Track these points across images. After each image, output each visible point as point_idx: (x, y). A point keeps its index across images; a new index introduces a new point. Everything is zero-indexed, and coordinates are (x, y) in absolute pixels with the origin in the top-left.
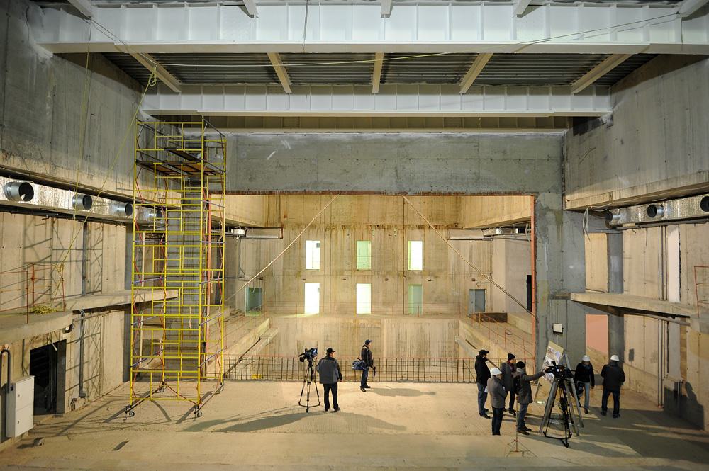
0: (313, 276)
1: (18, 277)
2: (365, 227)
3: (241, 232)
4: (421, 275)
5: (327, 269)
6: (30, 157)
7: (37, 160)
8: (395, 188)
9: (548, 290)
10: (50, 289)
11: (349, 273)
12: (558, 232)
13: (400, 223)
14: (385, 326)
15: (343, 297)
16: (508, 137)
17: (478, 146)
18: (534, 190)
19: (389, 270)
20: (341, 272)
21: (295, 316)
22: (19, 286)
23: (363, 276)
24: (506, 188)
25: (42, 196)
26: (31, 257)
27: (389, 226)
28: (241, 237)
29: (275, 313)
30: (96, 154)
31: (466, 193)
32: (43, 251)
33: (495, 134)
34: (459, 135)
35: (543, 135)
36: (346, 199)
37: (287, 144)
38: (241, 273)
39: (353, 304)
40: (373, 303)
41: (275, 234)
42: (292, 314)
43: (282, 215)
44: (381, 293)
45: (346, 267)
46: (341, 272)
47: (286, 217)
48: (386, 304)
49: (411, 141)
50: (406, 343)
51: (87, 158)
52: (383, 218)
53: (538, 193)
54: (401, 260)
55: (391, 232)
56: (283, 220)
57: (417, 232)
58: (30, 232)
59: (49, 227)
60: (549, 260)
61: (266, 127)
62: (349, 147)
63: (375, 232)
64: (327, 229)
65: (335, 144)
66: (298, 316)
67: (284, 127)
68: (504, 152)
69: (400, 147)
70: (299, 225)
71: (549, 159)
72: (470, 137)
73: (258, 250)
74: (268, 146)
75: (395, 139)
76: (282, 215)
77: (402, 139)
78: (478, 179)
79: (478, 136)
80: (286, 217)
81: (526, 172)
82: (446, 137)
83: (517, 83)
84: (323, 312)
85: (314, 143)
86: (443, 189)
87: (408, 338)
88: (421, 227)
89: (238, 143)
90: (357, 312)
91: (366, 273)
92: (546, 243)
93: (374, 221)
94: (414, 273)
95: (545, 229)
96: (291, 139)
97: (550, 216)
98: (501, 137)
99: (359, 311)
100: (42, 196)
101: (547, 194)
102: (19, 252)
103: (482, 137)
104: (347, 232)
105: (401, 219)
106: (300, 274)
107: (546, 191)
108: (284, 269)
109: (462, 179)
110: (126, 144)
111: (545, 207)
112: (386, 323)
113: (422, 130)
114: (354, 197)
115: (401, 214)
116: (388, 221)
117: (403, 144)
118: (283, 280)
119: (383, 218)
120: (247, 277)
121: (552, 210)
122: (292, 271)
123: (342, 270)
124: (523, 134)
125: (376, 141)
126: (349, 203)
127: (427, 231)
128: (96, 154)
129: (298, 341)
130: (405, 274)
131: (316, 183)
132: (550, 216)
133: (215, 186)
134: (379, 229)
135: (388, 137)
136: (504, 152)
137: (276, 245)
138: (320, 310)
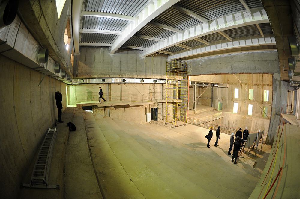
0: (236, 100)
1: (148, 95)
2: (251, 85)
3: (217, 85)
4: (268, 103)
5: (240, 98)
6: (142, 75)
7: (143, 75)
8: (231, 72)
9: (275, 111)
10: (155, 98)
11: (246, 100)
12: (280, 89)
13: (262, 84)
14: (253, 120)
15: (244, 108)
16: (262, 52)
17: (254, 56)
18: (272, 72)
19: (258, 100)
20: (244, 100)
21: (228, 113)
22: (149, 97)
23: (251, 102)
24: (264, 71)
25: (146, 81)
26: (150, 91)
27: (259, 84)
28: (217, 87)
29: (225, 111)
30: (156, 72)
31: (252, 73)
32: (153, 90)
33: (258, 52)
34: (248, 53)
35: (272, 51)
36: (246, 75)
37: (203, 61)
38: (217, 98)
39: (247, 111)
40: (253, 112)
41: (225, 86)
42: (229, 112)
43: (228, 80)
44: (255, 109)
45: (246, 98)
46: (244, 100)
47: (229, 80)
48: (256, 112)
49: (234, 56)
50: (258, 127)
51: (154, 73)
52: (257, 82)
53: (273, 73)
54: (262, 97)
55: (259, 87)
56: (228, 81)
57: (267, 87)
58: (150, 87)
59: (154, 86)
60: (277, 100)
61: (198, 57)
62: (218, 60)
63: (255, 86)
64: (240, 86)
65: (215, 59)
66: (232, 113)
67: (196, 57)
68: (262, 58)
69: (232, 58)
70: (232, 83)
71: (275, 60)
72: (251, 53)
73: (222, 91)
74: (199, 62)
75: (230, 56)
76: (228, 80)
77: (232, 56)
78: (255, 68)
79: (254, 53)
80: (229, 80)
81: (269, 65)
82: (244, 54)
83: (240, 37)
84: (238, 113)
85: (210, 60)
86: (245, 72)
87: (259, 125)
88: (268, 85)
89: (194, 62)
90: (248, 114)
91: (251, 101)
92: (276, 93)
93: (254, 83)
94: (265, 102)
95: (276, 88)
96: (204, 59)
97: (277, 82)
98: (260, 53)
99: (249, 114)
100: (146, 81)
101: (276, 74)
102: (148, 91)
103: (254, 53)
104: (246, 86)
105: (262, 82)
106: (233, 99)
107: (275, 73)
108: (228, 97)
109: (250, 68)
110: (164, 68)
111: (276, 79)
112: (254, 119)
113: (237, 52)
114: (248, 75)
115: (262, 80)
116: (258, 83)
117: (232, 57)
118: (228, 101)
119: (257, 82)
120: (219, 99)
121: (278, 80)
122: (230, 98)
123: (244, 99)
124: (267, 51)
125: (225, 57)
126: (247, 76)
127: (270, 87)
128: (156, 72)
129: (229, 120)
130: (263, 102)
131: (211, 71)
132: (277, 82)
133: (189, 74)
134: (256, 85)
135: (228, 56)
136: (262, 58)
137: (226, 89)
138: (238, 111)
